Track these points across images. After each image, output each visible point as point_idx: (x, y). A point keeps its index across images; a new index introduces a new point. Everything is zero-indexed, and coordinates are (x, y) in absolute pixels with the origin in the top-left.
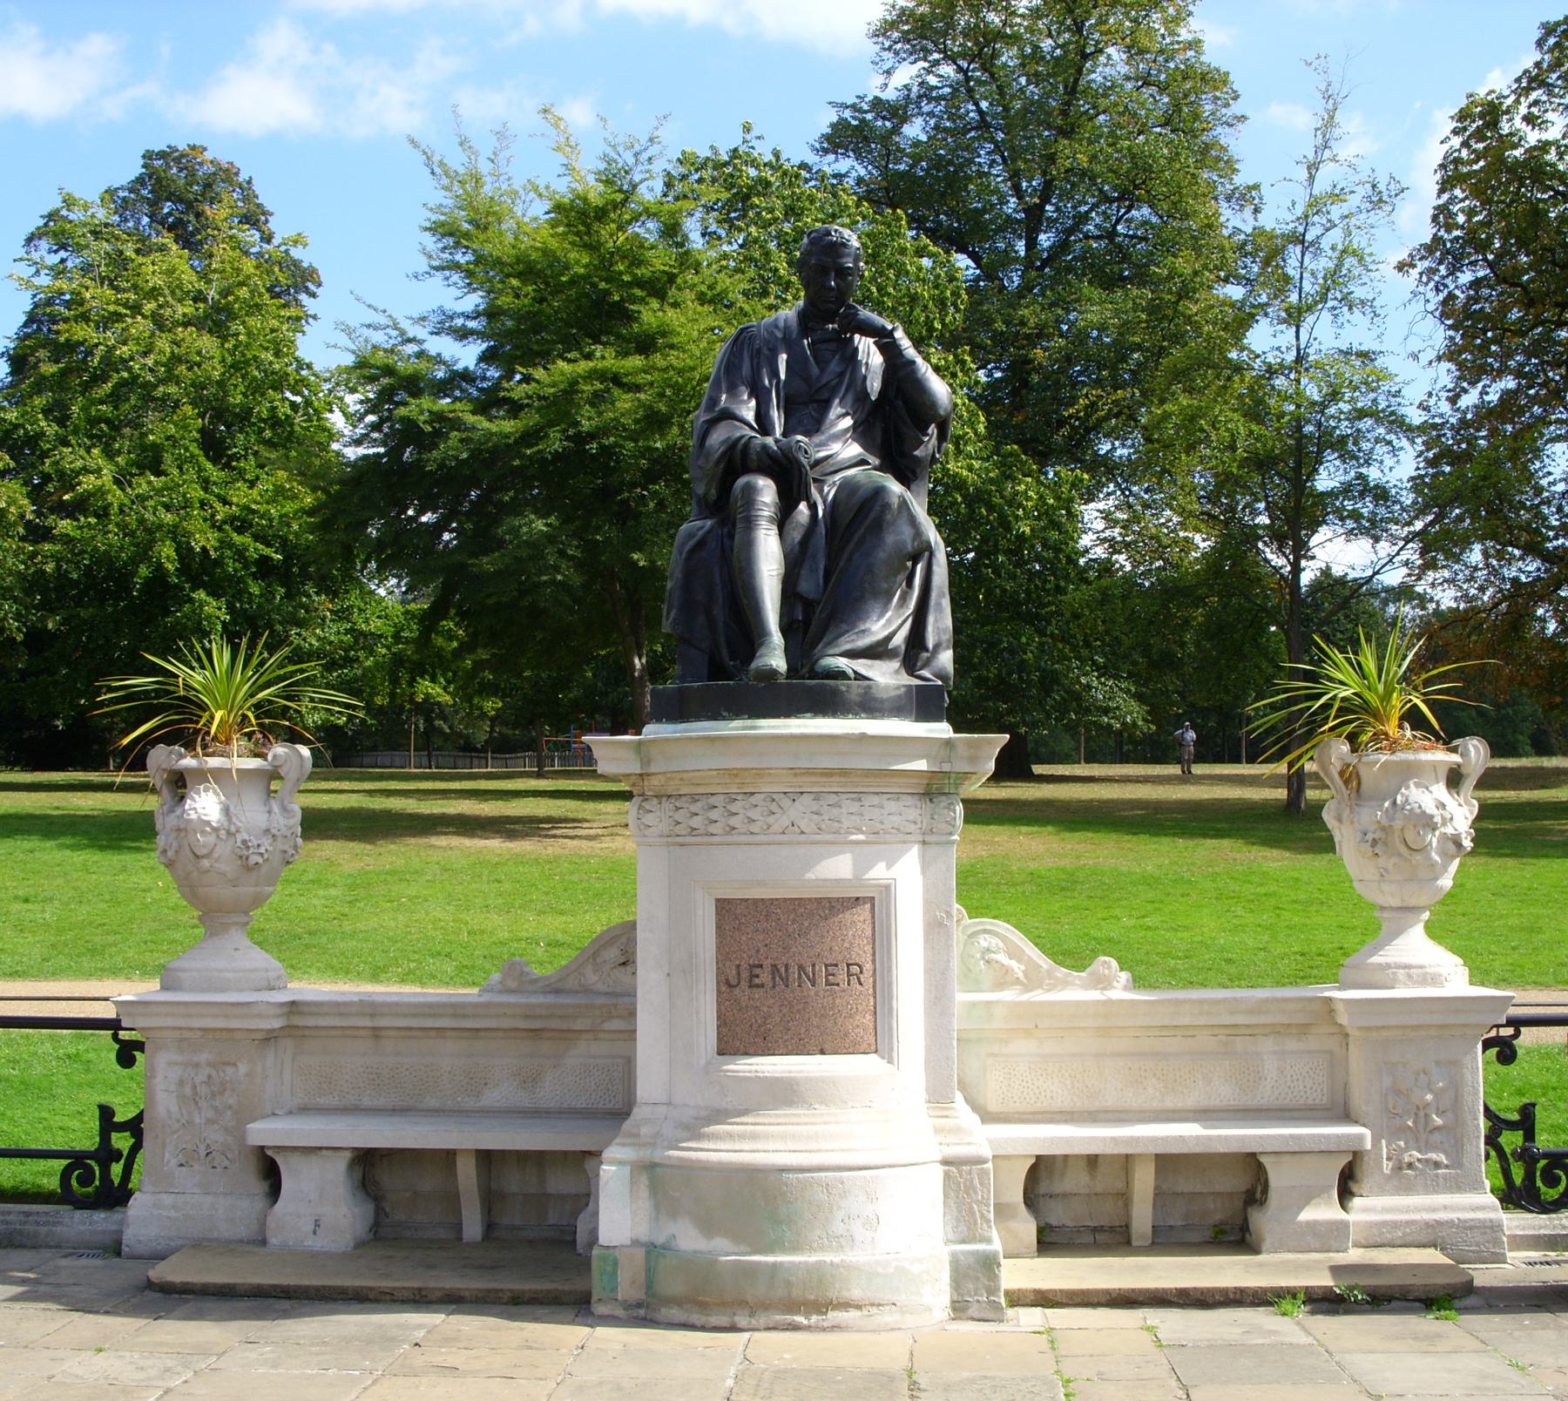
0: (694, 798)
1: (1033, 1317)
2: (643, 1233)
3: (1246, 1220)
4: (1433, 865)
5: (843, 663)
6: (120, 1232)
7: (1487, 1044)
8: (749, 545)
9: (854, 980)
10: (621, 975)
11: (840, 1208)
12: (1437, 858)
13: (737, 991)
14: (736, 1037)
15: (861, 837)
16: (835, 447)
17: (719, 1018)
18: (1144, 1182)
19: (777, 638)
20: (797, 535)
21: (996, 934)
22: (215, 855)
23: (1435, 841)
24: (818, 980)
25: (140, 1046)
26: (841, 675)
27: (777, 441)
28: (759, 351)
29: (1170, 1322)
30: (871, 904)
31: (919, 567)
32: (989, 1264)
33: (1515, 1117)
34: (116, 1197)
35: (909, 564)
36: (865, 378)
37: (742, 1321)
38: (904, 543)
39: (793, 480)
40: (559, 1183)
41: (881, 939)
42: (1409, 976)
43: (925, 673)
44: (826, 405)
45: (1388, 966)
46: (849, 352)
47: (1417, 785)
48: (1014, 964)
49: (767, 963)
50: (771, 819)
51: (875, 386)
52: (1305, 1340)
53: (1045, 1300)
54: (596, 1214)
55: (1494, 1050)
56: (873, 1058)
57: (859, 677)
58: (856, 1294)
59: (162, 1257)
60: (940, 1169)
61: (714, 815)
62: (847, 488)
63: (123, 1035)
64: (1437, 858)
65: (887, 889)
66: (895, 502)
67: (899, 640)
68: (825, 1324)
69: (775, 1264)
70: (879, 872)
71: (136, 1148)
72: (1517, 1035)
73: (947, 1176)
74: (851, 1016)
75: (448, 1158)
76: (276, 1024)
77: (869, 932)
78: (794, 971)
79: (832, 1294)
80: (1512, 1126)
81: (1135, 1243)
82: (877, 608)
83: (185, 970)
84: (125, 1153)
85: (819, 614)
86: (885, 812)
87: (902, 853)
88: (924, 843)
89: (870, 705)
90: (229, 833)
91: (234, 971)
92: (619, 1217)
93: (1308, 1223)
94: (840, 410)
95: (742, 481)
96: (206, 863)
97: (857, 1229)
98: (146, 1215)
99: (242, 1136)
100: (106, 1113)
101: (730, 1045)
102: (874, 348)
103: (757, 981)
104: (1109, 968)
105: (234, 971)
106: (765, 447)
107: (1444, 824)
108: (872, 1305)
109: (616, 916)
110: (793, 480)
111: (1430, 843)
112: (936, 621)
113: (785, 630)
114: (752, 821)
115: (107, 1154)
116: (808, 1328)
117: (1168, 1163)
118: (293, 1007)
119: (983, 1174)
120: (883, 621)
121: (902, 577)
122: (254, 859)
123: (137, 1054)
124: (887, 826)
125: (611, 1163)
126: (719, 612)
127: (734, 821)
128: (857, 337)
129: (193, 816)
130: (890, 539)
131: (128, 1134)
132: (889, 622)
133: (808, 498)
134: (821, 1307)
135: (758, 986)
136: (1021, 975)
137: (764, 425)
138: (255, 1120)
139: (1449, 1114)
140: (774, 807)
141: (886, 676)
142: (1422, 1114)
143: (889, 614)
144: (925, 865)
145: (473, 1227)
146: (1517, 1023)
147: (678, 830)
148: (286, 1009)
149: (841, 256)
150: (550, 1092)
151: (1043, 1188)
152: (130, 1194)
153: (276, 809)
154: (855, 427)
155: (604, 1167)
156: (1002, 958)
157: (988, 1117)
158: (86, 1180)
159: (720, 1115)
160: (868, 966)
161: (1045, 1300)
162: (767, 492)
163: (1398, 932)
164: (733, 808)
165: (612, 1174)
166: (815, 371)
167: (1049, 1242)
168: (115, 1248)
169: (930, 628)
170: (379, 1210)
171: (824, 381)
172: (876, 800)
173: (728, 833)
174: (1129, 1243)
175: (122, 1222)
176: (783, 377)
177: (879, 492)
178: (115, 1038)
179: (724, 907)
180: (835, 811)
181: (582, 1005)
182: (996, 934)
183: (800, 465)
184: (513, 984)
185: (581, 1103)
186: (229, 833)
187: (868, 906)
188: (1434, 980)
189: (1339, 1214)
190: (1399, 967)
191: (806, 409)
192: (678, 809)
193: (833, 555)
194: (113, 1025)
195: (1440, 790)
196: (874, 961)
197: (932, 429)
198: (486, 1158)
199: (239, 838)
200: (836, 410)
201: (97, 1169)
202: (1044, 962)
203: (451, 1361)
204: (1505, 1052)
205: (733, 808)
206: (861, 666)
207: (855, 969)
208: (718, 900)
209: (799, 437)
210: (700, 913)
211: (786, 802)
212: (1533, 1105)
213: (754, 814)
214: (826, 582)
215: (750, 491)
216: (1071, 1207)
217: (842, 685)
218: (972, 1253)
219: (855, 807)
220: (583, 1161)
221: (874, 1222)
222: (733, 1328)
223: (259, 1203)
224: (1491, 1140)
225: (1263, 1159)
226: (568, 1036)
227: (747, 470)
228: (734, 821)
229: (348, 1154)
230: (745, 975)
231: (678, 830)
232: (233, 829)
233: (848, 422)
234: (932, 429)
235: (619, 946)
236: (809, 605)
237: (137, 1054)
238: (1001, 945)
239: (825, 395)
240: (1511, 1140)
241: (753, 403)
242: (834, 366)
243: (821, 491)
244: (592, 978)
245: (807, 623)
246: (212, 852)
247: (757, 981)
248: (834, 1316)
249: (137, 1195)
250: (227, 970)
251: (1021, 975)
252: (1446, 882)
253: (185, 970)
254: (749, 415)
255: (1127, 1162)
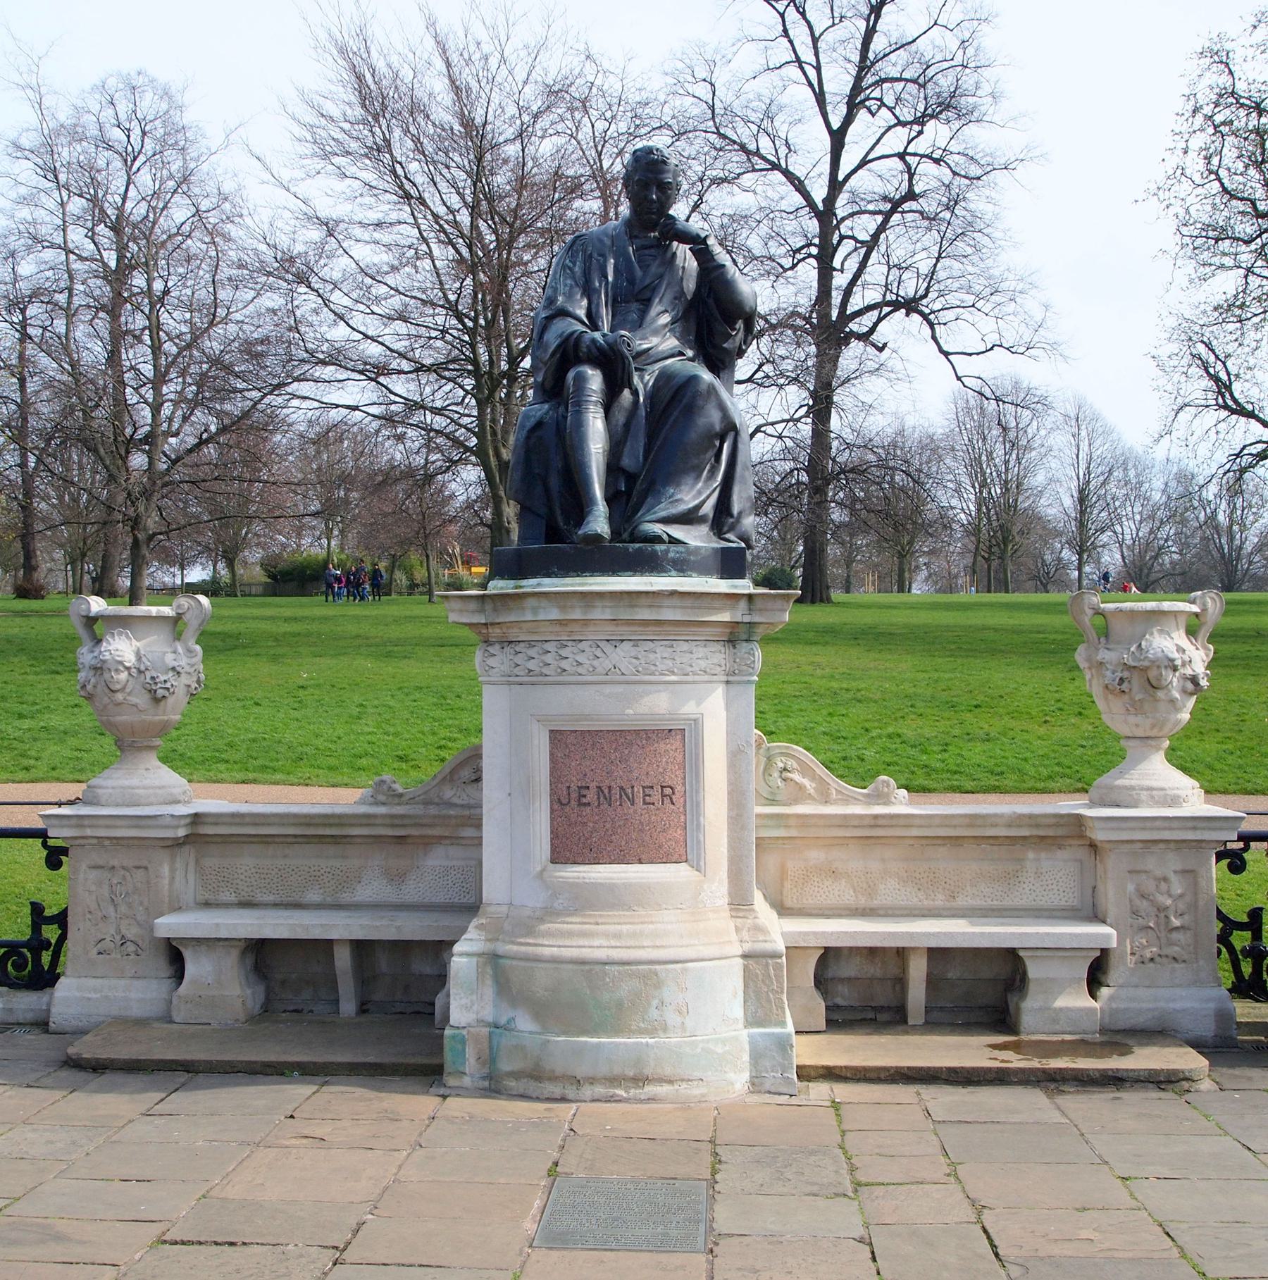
0: (531, 644)
1: (820, 1091)
2: (488, 1014)
3: (1006, 1002)
4: (1172, 701)
5: (658, 528)
6: (48, 1011)
7: (1220, 856)
8: (579, 424)
9: (667, 800)
10: (470, 789)
11: (654, 997)
12: (1178, 696)
13: (567, 809)
14: (566, 849)
15: (673, 678)
16: (655, 341)
17: (552, 832)
18: (918, 970)
19: (601, 508)
20: (620, 418)
21: (793, 757)
22: (128, 690)
23: (1175, 680)
24: (637, 800)
25: (65, 851)
26: (657, 539)
27: (604, 335)
28: (591, 256)
29: (943, 1099)
30: (678, 736)
31: (726, 445)
32: (783, 1045)
33: (1245, 919)
34: (45, 980)
35: (717, 443)
36: (682, 279)
37: (570, 1092)
38: (712, 426)
39: (616, 368)
40: (421, 966)
41: (691, 763)
42: (1152, 797)
43: (730, 536)
44: (646, 303)
45: (1132, 788)
46: (669, 255)
47: (1161, 632)
48: (806, 782)
49: (593, 785)
50: (595, 663)
51: (690, 285)
52: (1057, 1117)
53: (831, 1074)
54: (448, 995)
55: (1225, 862)
56: (683, 866)
57: (673, 541)
58: (668, 1071)
59: (83, 1032)
60: (741, 961)
61: (549, 658)
62: (665, 378)
63: (51, 842)
64: (1178, 696)
65: (696, 723)
66: (703, 387)
67: (708, 509)
68: (642, 1097)
69: (599, 1044)
70: (689, 708)
71: (62, 938)
72: (1246, 848)
73: (746, 969)
74: (664, 831)
75: (324, 947)
76: (181, 833)
77: (680, 758)
78: (616, 791)
79: (648, 1071)
80: (1241, 926)
81: (910, 1022)
82: (689, 480)
83: (100, 787)
84: (53, 941)
85: (639, 486)
86: (695, 656)
87: (713, 691)
88: (727, 682)
89: (682, 566)
90: (140, 672)
91: (144, 788)
92: (466, 1005)
93: (1061, 1009)
94: (660, 308)
95: (571, 375)
96: (120, 697)
97: (672, 1018)
98: (72, 996)
99: (151, 929)
100: (37, 909)
101: (562, 853)
102: (689, 253)
103: (584, 800)
104: (888, 785)
105: (144, 788)
106: (594, 341)
107: (1184, 665)
108: (683, 1080)
109: (464, 743)
110: (616, 368)
111: (1171, 682)
112: (740, 492)
113: (609, 500)
114: (579, 664)
115: (38, 944)
116: (626, 1100)
117: (938, 955)
118: (197, 818)
119: (778, 967)
120: (694, 492)
121: (711, 454)
122: (160, 693)
123: (64, 858)
124: (696, 668)
125: (461, 955)
126: (554, 482)
127: (564, 664)
128: (675, 243)
129: (107, 656)
130: (701, 422)
131: (56, 926)
132: (700, 493)
133: (630, 385)
134: (640, 1080)
135: (585, 804)
136: (812, 791)
137: (593, 320)
138: (162, 915)
139: (1186, 917)
140: (599, 653)
141: (697, 538)
142: (1162, 915)
143: (700, 485)
144: (728, 706)
145: (348, 1006)
146: (1246, 838)
147: (516, 671)
148: (188, 820)
149: (663, 172)
150: (413, 891)
151: (830, 974)
152: (58, 977)
153: (180, 650)
154: (673, 322)
155: (454, 959)
156: (796, 776)
157: (783, 910)
158: (19, 967)
159: (549, 913)
160: (679, 788)
161: (831, 1074)
162: (595, 380)
163: (1144, 758)
164: (564, 652)
165: (463, 960)
166: (639, 273)
167: (840, 1019)
168: (42, 1025)
169: (735, 498)
170: (268, 991)
171: (647, 281)
172: (685, 646)
173: (560, 674)
174: (906, 1022)
175: (49, 1004)
176: (610, 279)
177: (694, 379)
178: (45, 845)
179: (556, 737)
180: (652, 656)
181: (437, 819)
182: (793, 757)
183: (623, 357)
184: (382, 798)
185: (441, 898)
186: (140, 672)
187: (679, 737)
188: (1174, 801)
189: (1089, 1003)
190: (1142, 789)
191: (632, 300)
192: (517, 653)
193: (651, 437)
194: (41, 834)
195: (1180, 638)
196: (684, 784)
197: (740, 324)
198: (361, 948)
199: (148, 675)
200: (656, 308)
201: (29, 955)
202: (835, 783)
203: (318, 1133)
204: (1236, 863)
205: (564, 652)
206: (677, 532)
207: (668, 791)
208: (551, 731)
209: (623, 332)
210: (536, 742)
211: (608, 648)
212: (1261, 909)
213: (580, 658)
214: (646, 458)
215: (581, 380)
216: (858, 991)
217: (660, 548)
218: (768, 1035)
219: (667, 652)
220: (441, 949)
221: (683, 1010)
222: (563, 1099)
223: (168, 984)
224: (1224, 939)
225: (1021, 953)
226: (427, 843)
227: (579, 361)
228: (564, 664)
229: (242, 944)
230: (574, 795)
231: (516, 671)
232: (143, 668)
233: (665, 319)
234: (740, 324)
235: (468, 769)
236: (631, 478)
237: (64, 858)
238: (795, 765)
239: (647, 294)
240: (1241, 940)
241: (585, 302)
242: (654, 269)
243: (642, 378)
244: (448, 793)
245: (629, 493)
246: (124, 688)
247: (584, 800)
248: (650, 1090)
249: (62, 979)
250: (138, 788)
251: (812, 791)
252: (1185, 716)
253: (100, 787)
254: (582, 313)
255: (901, 953)
